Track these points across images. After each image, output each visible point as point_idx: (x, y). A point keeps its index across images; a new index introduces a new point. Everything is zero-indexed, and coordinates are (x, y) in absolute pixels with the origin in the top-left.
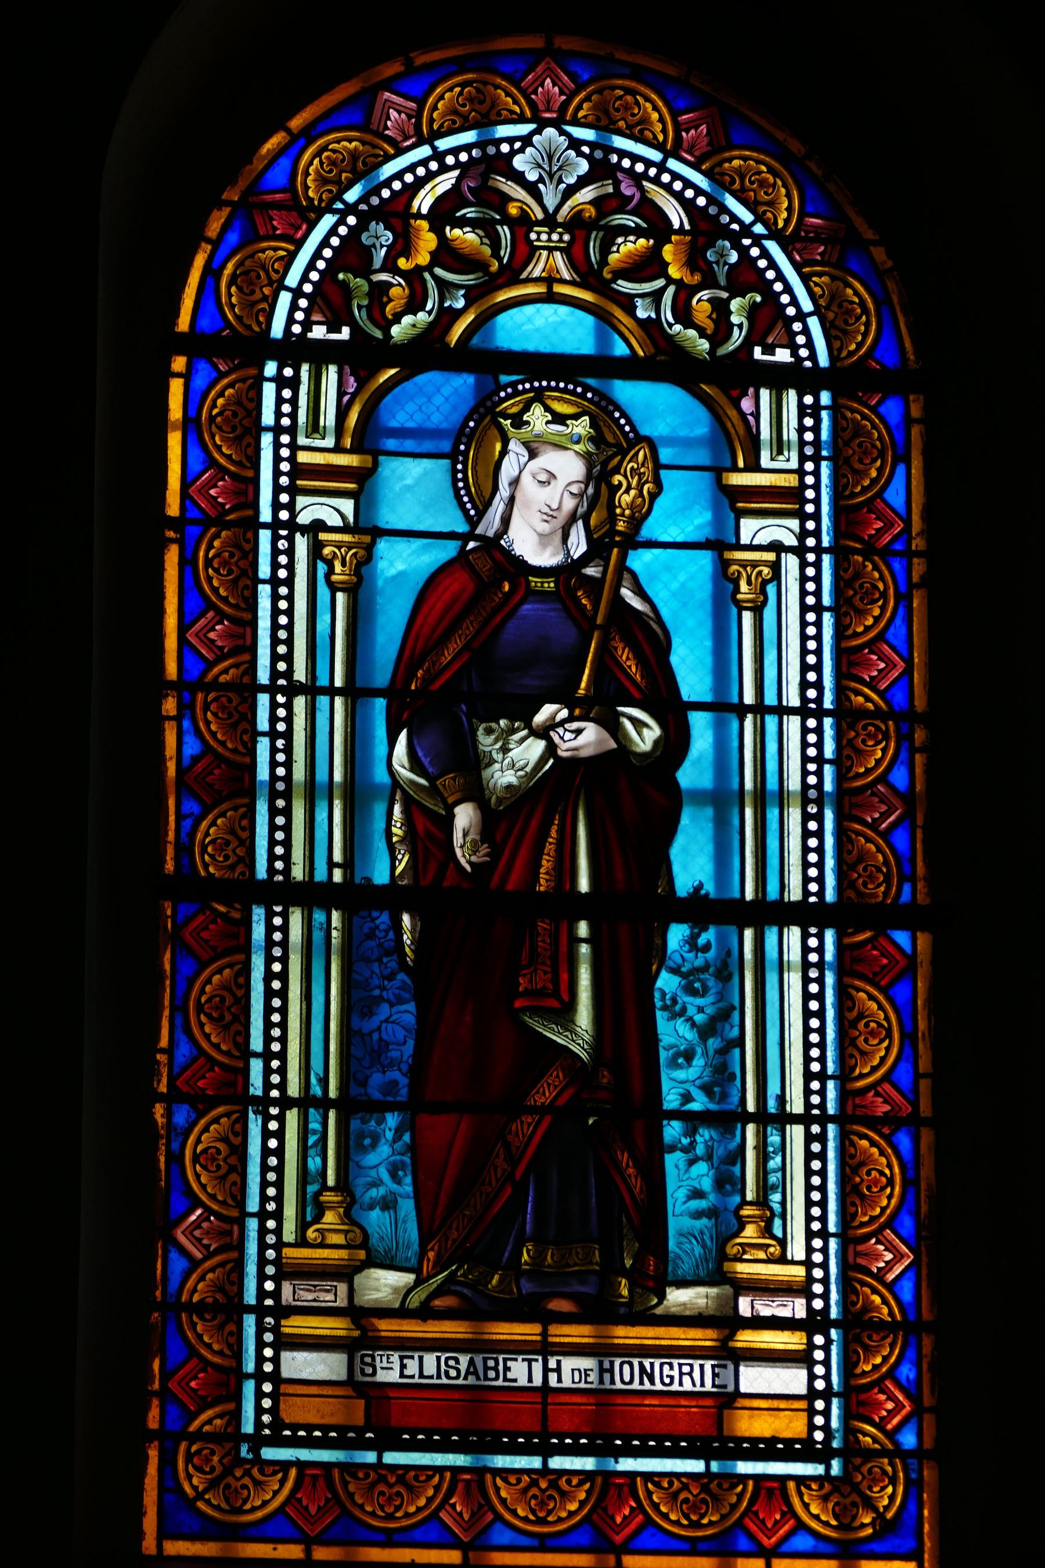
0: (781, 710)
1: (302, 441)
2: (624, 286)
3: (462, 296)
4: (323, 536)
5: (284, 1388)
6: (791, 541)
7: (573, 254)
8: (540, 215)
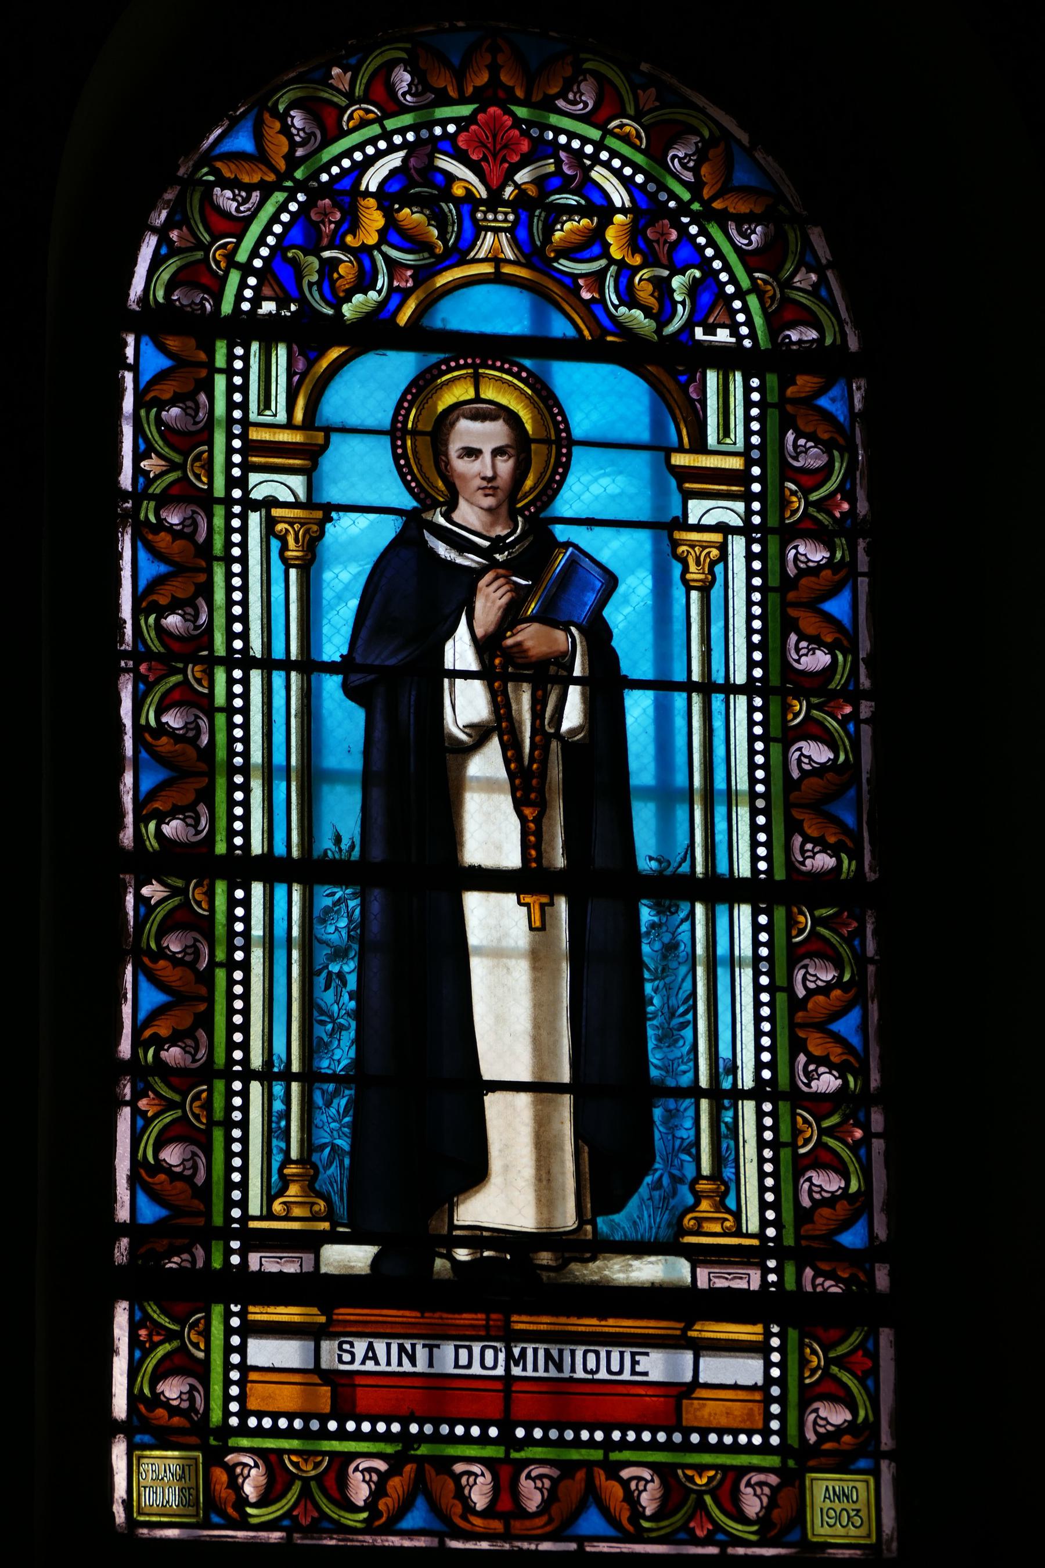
0: (729, 689)
1: (253, 416)
2: (565, 265)
4: (276, 512)
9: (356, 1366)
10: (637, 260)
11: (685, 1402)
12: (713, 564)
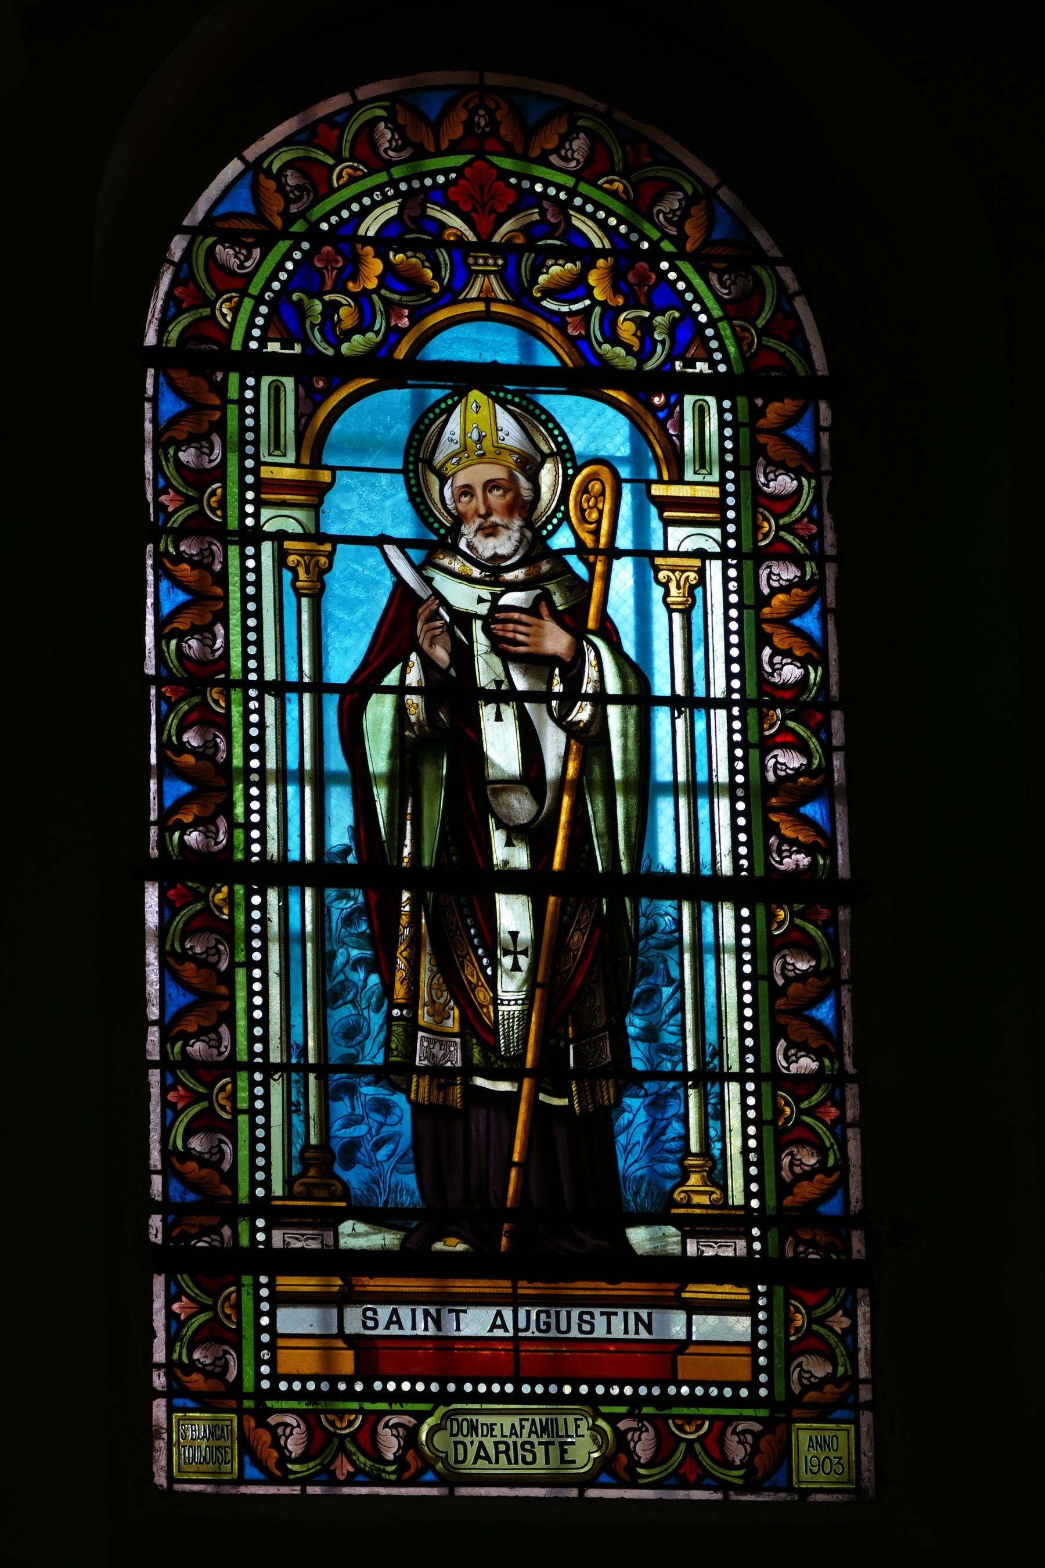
0: (709, 703)
1: (265, 458)
4: (288, 545)
5: (281, 1343)
7: (508, 277)
9: (380, 1331)
11: (680, 1358)
12: (692, 588)
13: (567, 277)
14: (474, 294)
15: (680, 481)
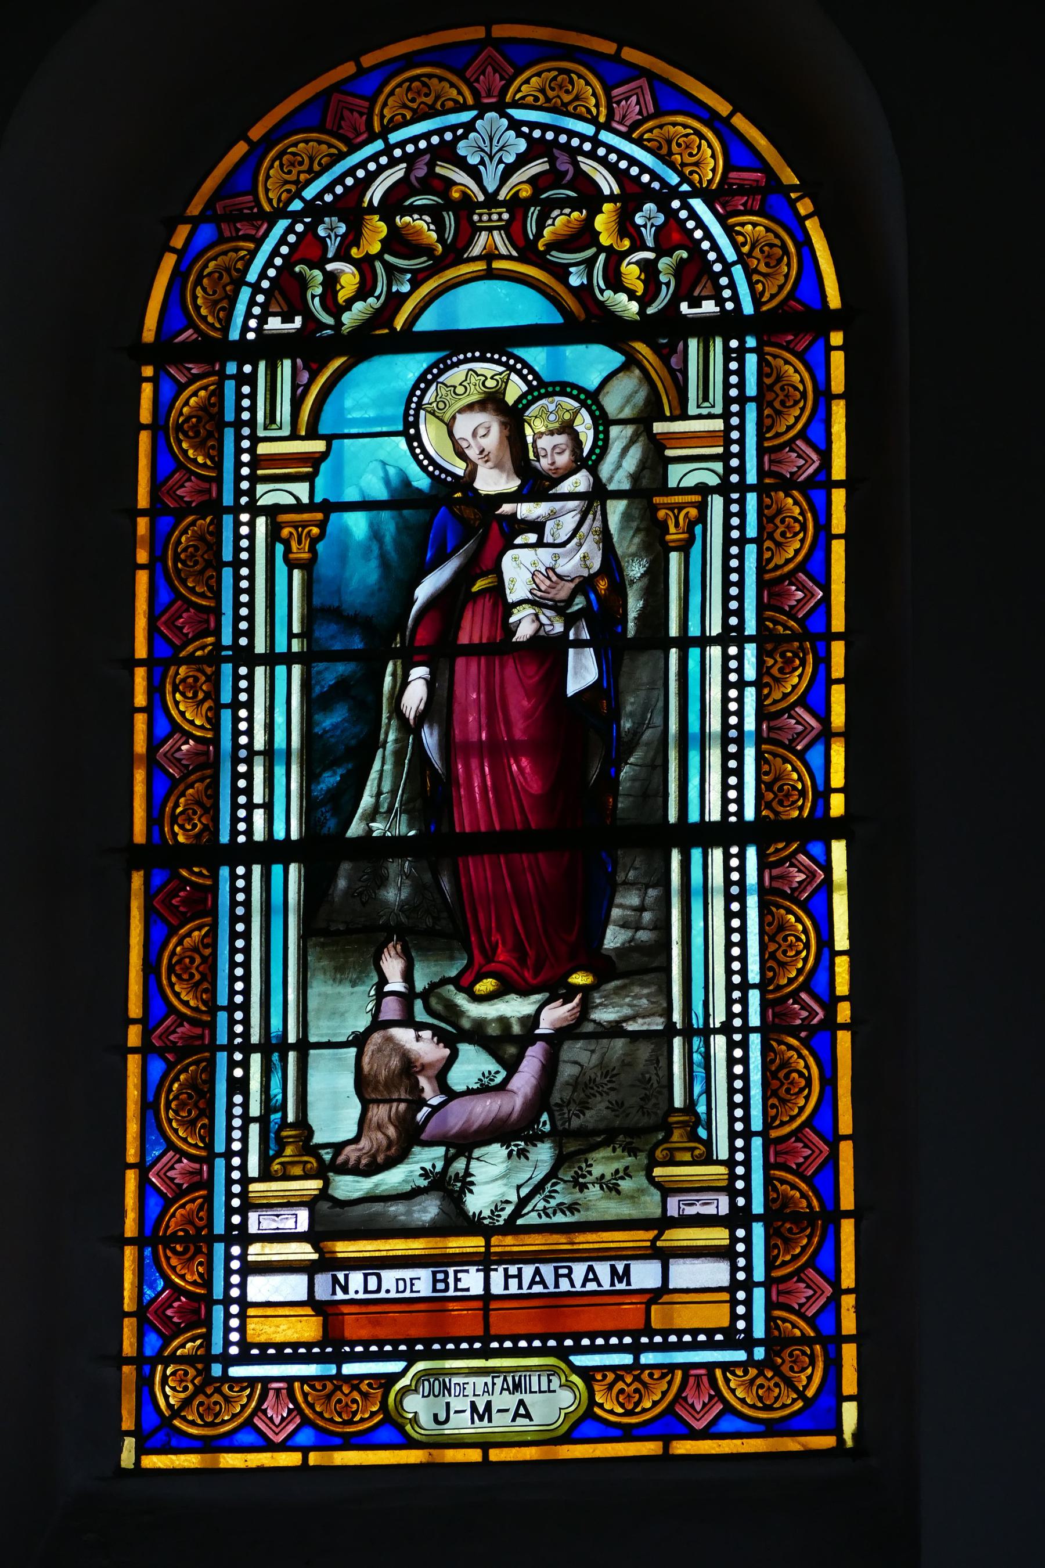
1: (261, 433)
2: (558, 257)
3: (408, 281)
6: (713, 481)
7: (513, 230)
8: (481, 198)
10: (627, 243)
12: (691, 525)
13: (575, 225)
14: (476, 251)
15: (684, 416)
